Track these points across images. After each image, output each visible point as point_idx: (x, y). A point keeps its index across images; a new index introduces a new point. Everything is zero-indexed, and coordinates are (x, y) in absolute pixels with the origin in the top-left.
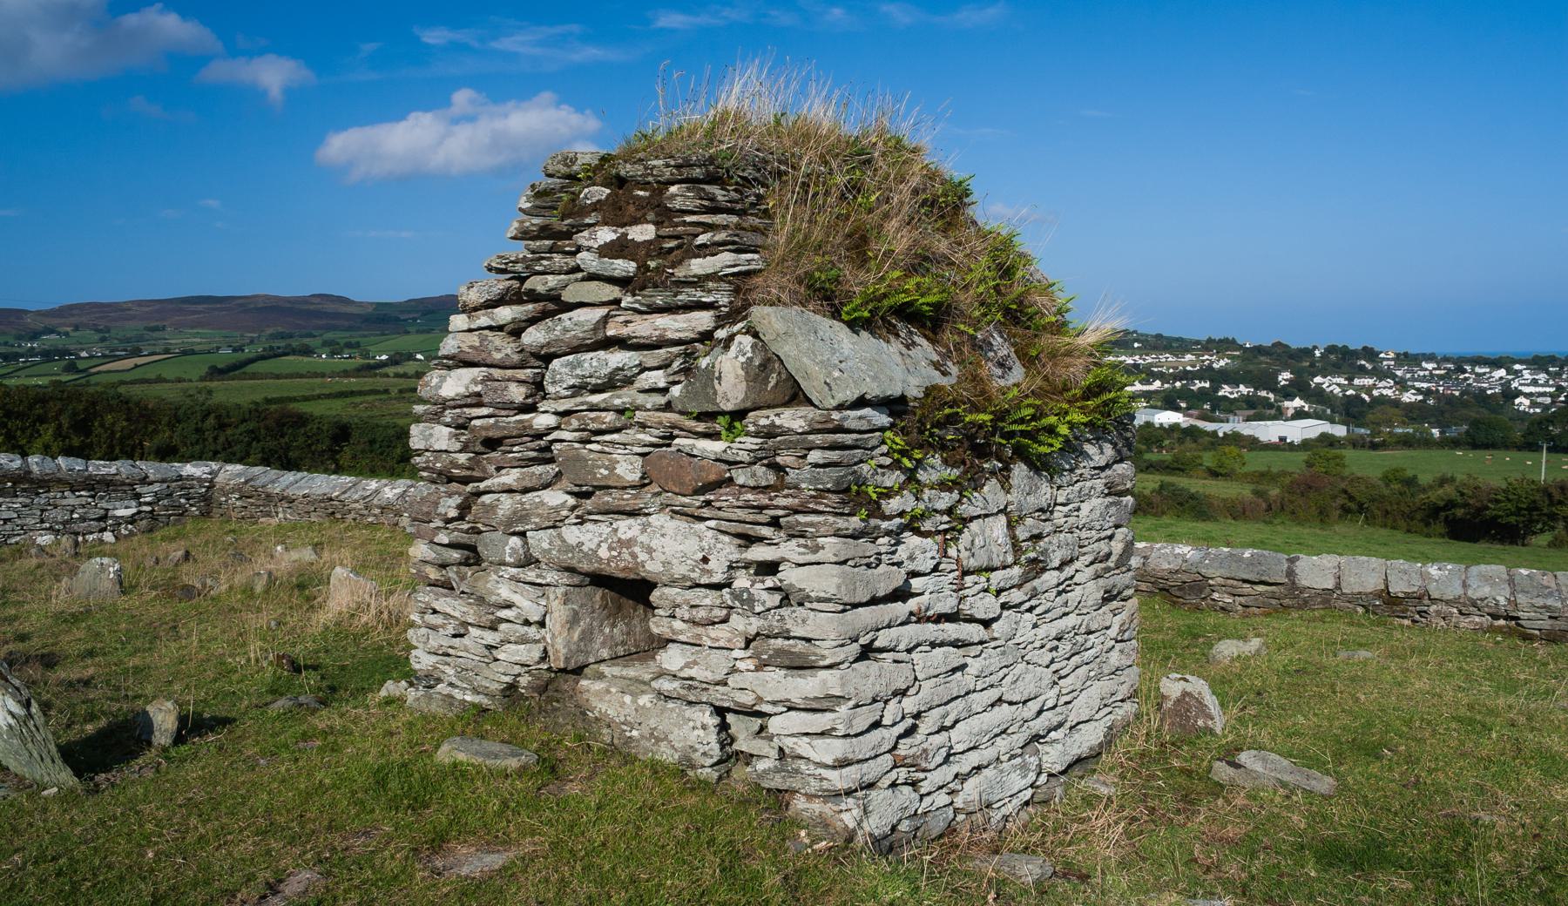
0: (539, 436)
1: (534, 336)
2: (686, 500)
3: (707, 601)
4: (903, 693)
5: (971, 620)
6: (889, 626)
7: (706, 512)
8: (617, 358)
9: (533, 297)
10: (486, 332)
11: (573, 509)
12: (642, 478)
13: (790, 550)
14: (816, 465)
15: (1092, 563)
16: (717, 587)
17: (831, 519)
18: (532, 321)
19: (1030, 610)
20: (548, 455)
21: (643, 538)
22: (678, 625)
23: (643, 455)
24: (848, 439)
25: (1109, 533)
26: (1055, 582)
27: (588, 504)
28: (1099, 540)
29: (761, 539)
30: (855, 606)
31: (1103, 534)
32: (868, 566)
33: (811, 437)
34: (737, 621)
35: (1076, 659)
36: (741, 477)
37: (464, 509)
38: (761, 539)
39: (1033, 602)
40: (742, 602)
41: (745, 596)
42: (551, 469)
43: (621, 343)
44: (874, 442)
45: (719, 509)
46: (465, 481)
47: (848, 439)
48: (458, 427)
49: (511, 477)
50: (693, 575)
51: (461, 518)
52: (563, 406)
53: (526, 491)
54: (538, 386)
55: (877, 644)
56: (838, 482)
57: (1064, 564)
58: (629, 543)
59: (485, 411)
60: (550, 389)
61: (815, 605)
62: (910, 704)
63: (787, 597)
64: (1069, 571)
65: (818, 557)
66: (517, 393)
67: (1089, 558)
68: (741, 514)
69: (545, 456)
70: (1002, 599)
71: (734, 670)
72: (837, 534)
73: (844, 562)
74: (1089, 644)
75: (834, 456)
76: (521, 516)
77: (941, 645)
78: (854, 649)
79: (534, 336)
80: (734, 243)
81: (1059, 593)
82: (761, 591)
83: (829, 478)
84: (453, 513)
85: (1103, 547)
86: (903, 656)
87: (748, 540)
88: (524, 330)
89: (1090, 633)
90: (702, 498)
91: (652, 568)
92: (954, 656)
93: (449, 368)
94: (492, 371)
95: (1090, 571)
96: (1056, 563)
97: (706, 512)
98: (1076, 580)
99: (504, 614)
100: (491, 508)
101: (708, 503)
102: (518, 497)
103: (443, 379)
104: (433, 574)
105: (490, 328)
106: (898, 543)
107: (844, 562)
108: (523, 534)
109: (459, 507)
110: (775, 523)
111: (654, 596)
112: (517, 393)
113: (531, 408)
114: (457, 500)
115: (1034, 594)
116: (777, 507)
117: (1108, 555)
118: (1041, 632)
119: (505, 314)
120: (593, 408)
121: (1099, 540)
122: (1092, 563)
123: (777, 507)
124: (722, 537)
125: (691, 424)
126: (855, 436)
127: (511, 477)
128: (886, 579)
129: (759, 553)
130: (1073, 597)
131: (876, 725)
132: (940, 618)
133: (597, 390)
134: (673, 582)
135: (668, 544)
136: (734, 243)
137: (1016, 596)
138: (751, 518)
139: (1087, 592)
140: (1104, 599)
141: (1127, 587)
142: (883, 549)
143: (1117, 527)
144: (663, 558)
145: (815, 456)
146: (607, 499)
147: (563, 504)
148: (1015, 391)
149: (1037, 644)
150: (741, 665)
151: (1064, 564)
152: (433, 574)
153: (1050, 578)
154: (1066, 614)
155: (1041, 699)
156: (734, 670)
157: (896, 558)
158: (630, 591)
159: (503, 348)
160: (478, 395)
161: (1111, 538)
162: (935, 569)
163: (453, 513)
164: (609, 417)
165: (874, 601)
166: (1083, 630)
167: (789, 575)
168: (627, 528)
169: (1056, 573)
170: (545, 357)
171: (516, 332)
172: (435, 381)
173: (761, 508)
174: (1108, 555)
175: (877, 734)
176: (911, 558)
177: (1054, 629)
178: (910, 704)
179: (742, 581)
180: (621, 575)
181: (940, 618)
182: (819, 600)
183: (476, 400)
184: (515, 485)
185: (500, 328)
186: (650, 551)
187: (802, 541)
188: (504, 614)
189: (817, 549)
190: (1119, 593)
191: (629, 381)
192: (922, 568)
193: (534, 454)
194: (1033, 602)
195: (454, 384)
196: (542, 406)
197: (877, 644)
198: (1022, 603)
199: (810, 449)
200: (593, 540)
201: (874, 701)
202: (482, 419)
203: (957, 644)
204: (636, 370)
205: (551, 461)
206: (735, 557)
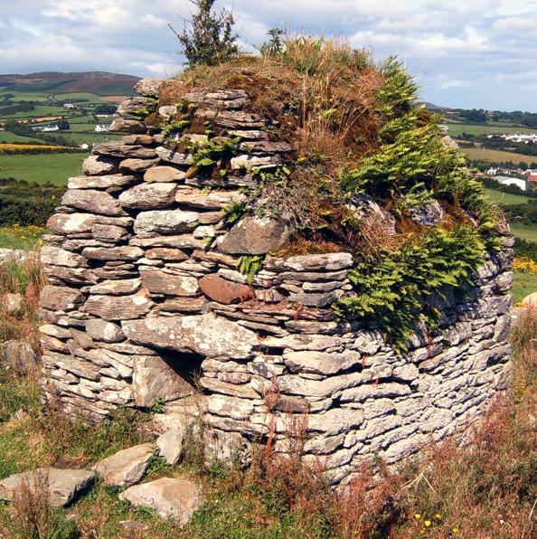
0: (130, 261)
1: (127, 197)
2: (226, 307)
3: (238, 369)
4: (356, 427)
5: (401, 381)
6: (349, 387)
7: (238, 315)
8: (180, 216)
9: (126, 171)
10: (94, 191)
11: (151, 308)
12: (197, 292)
13: (287, 340)
14: (307, 292)
15: (481, 340)
16: (241, 361)
17: (317, 323)
18: (126, 187)
19: (440, 372)
20: (136, 273)
21: (198, 329)
22: (217, 382)
23: (199, 278)
24: (329, 275)
25: (493, 319)
26: (455, 354)
27: (162, 305)
28: (487, 324)
29: (273, 334)
30: (329, 376)
31: (490, 320)
32: (338, 351)
33: (306, 274)
34: (255, 384)
35: (469, 403)
36: (260, 294)
37: (78, 303)
38: (273, 334)
39: (440, 368)
40: (259, 370)
41: (261, 368)
42: (136, 282)
43: (185, 207)
44: (342, 277)
45: (246, 314)
46: (78, 286)
47: (329, 275)
48: (74, 251)
49: (110, 286)
50: (230, 353)
51: (76, 309)
52: (146, 243)
53: (121, 294)
54: (130, 229)
55: (342, 399)
56: (321, 302)
57: (462, 342)
58: (189, 331)
59: (93, 242)
60: (138, 231)
61: (305, 375)
62: (360, 435)
63: (290, 370)
64: (465, 347)
65: (310, 346)
66: (117, 233)
67: (479, 337)
68: (259, 318)
69: (134, 273)
70: (421, 366)
71: (254, 412)
72: (321, 332)
73: (324, 350)
74: (477, 393)
75: (319, 286)
76: (114, 311)
77: (381, 397)
78: (329, 401)
79: (127, 197)
80: (259, 151)
81: (458, 361)
82: (272, 365)
83: (315, 299)
84: (71, 306)
85: (489, 329)
86: (359, 405)
87: (263, 334)
88: (120, 192)
89: (478, 385)
90: (236, 306)
91: (203, 347)
92: (384, 404)
93: (69, 213)
94: (99, 217)
95: (479, 346)
96: (456, 342)
97: (238, 315)
98: (470, 351)
99: (104, 371)
100: (98, 304)
101: (238, 310)
102: (116, 298)
103: (64, 220)
104: (58, 344)
105: (97, 189)
106: (356, 337)
107: (324, 350)
108: (118, 323)
109: (75, 302)
110: (281, 324)
111: (204, 365)
112: (117, 233)
113: (126, 243)
114: (73, 297)
115: (443, 362)
116: (283, 315)
117: (491, 336)
118: (445, 385)
119: (107, 181)
120: (168, 246)
121: (487, 324)
122: (481, 340)
123: (283, 315)
124: (248, 331)
125: (229, 260)
126: (332, 274)
127: (110, 286)
128: (352, 358)
129: (271, 342)
130: (467, 364)
131: (341, 447)
132: (382, 381)
133: (167, 234)
134: (215, 357)
135: (212, 335)
136: (259, 151)
137: (429, 364)
138: (267, 320)
139: (478, 358)
140: (488, 362)
141: (505, 354)
142: (347, 341)
143: (499, 315)
144: (209, 341)
145: (307, 286)
146: (173, 303)
147: (145, 305)
148: (423, 106)
149: (442, 395)
150: (257, 409)
151: (462, 342)
152: (58, 344)
153: (452, 351)
154: (462, 374)
155: (445, 429)
156: (254, 412)
157: (355, 346)
158: (185, 363)
159: (106, 202)
160: (90, 231)
161: (494, 323)
162: (379, 350)
163: (71, 306)
164: (176, 252)
165: (341, 372)
166: (473, 383)
167: (290, 356)
168: (188, 321)
169: (456, 348)
170: (133, 211)
171: (115, 194)
172: (59, 221)
173: (272, 315)
174: (491, 336)
175: (340, 453)
176: (364, 345)
177: (453, 384)
178: (360, 435)
179: (260, 358)
180: (183, 351)
181: (382, 381)
182: (308, 372)
183: (88, 235)
184: (114, 291)
185: (103, 189)
186: (201, 336)
187: (298, 336)
188: (104, 371)
189: (308, 341)
190: (499, 358)
191: (191, 231)
192: (370, 351)
193: (127, 272)
194: (440, 368)
195: (75, 222)
196: (133, 241)
197: (342, 399)
198: (433, 369)
199: (304, 281)
200: (160, 327)
201: (340, 432)
202: (91, 247)
203: (392, 396)
204: (196, 224)
205: (138, 276)
206: (257, 343)
